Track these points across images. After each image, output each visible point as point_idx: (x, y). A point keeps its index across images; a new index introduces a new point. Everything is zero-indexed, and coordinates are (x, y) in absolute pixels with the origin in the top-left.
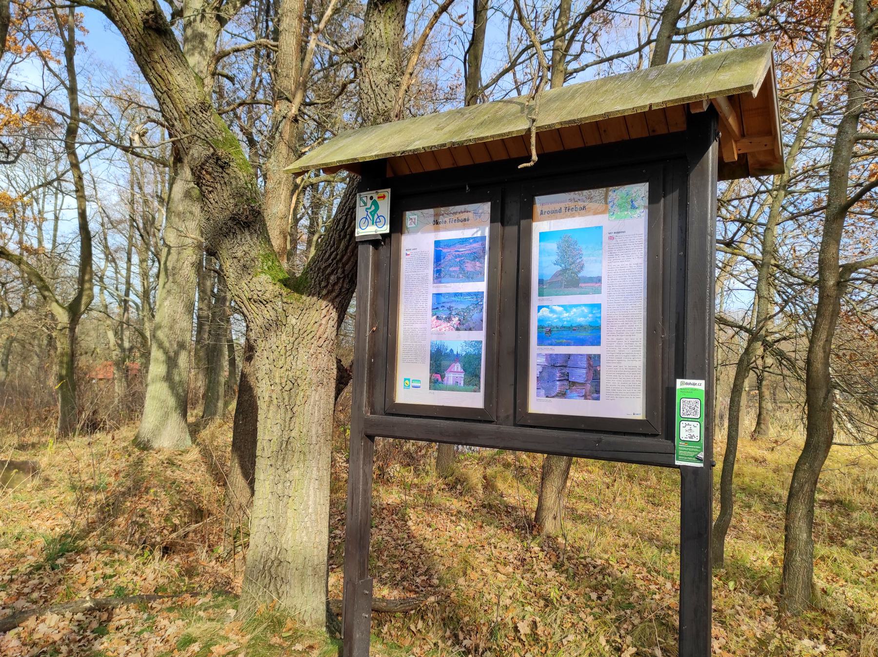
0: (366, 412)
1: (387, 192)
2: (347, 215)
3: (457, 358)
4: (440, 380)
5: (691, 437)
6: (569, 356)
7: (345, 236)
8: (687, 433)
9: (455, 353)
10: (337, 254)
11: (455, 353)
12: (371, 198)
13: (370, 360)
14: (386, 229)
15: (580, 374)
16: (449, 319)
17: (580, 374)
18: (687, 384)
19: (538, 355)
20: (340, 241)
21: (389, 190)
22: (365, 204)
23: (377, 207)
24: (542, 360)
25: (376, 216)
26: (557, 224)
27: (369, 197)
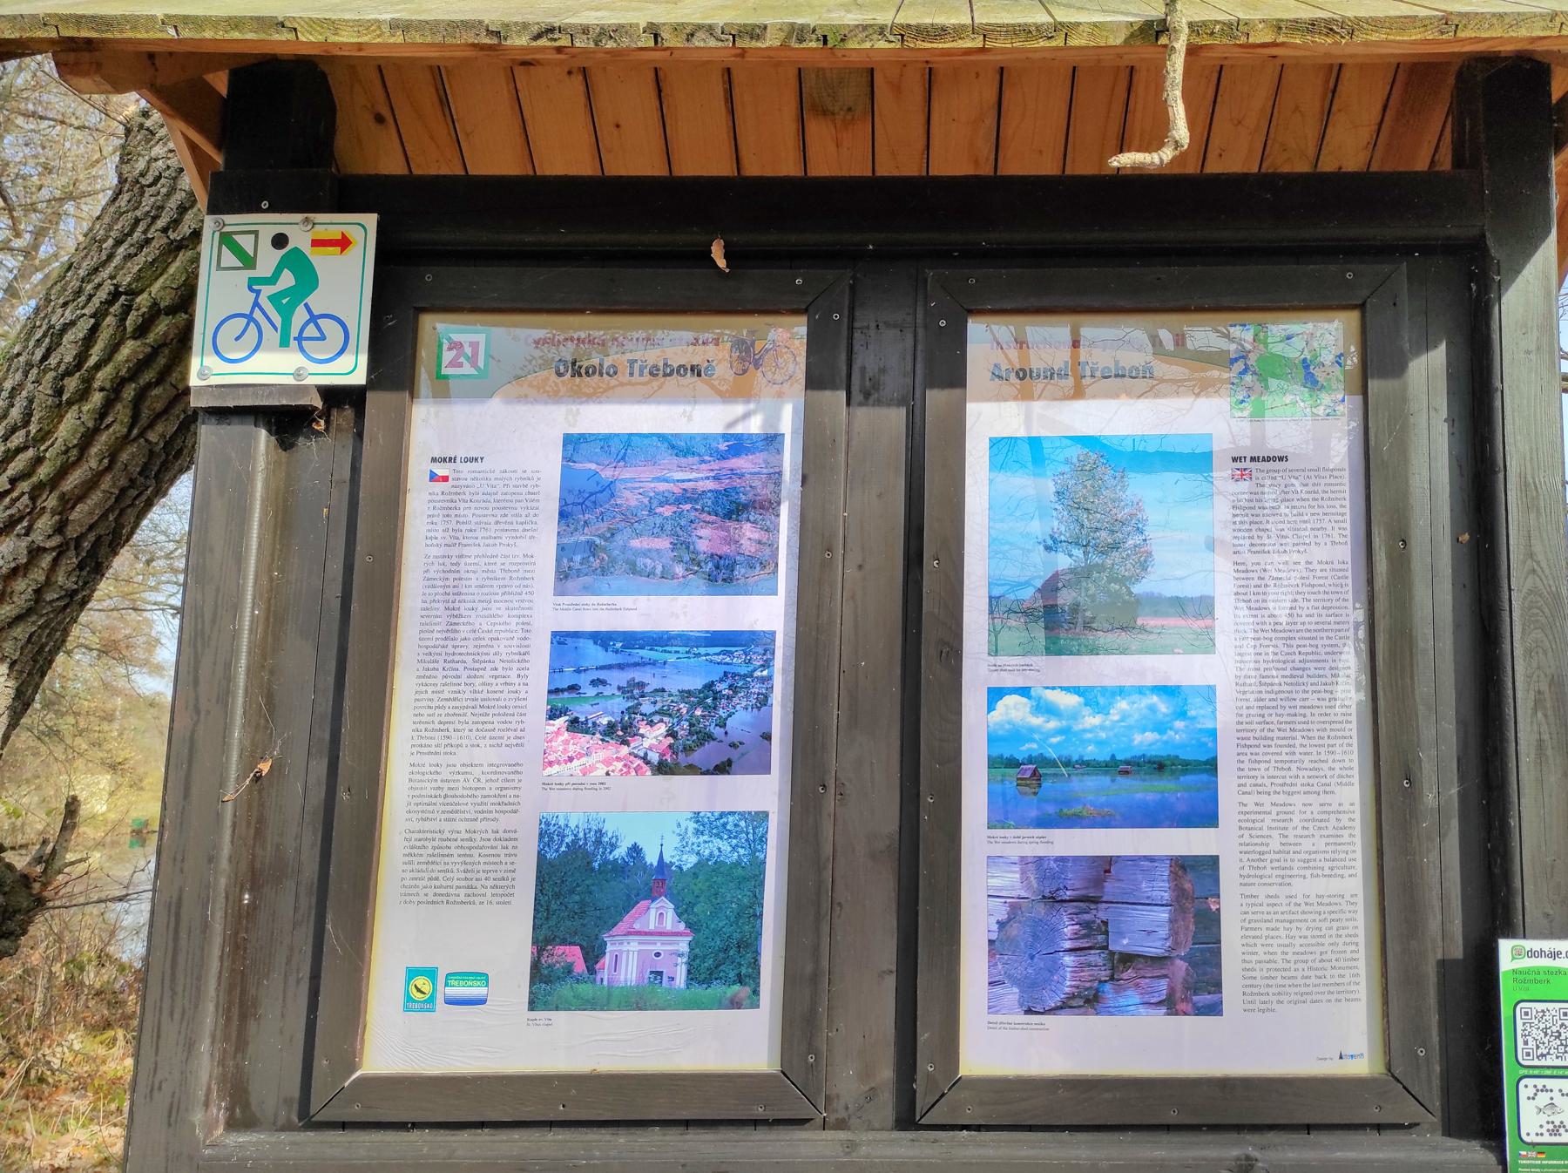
0: (210, 1127)
1: (363, 228)
2: (99, 316)
3: (659, 881)
4: (580, 967)
5: (1555, 1132)
6: (1105, 866)
7: (83, 395)
8: (1543, 1118)
9: (651, 858)
10: (38, 461)
11: (651, 858)
12: (280, 241)
13: (233, 899)
14: (352, 369)
15: (1147, 926)
16: (621, 731)
17: (1147, 926)
18: (1532, 954)
19: (992, 865)
20: (58, 410)
21: (371, 220)
22: (249, 262)
23: (307, 279)
24: (1010, 881)
25: (300, 316)
26: (1056, 418)
27: (267, 235)
